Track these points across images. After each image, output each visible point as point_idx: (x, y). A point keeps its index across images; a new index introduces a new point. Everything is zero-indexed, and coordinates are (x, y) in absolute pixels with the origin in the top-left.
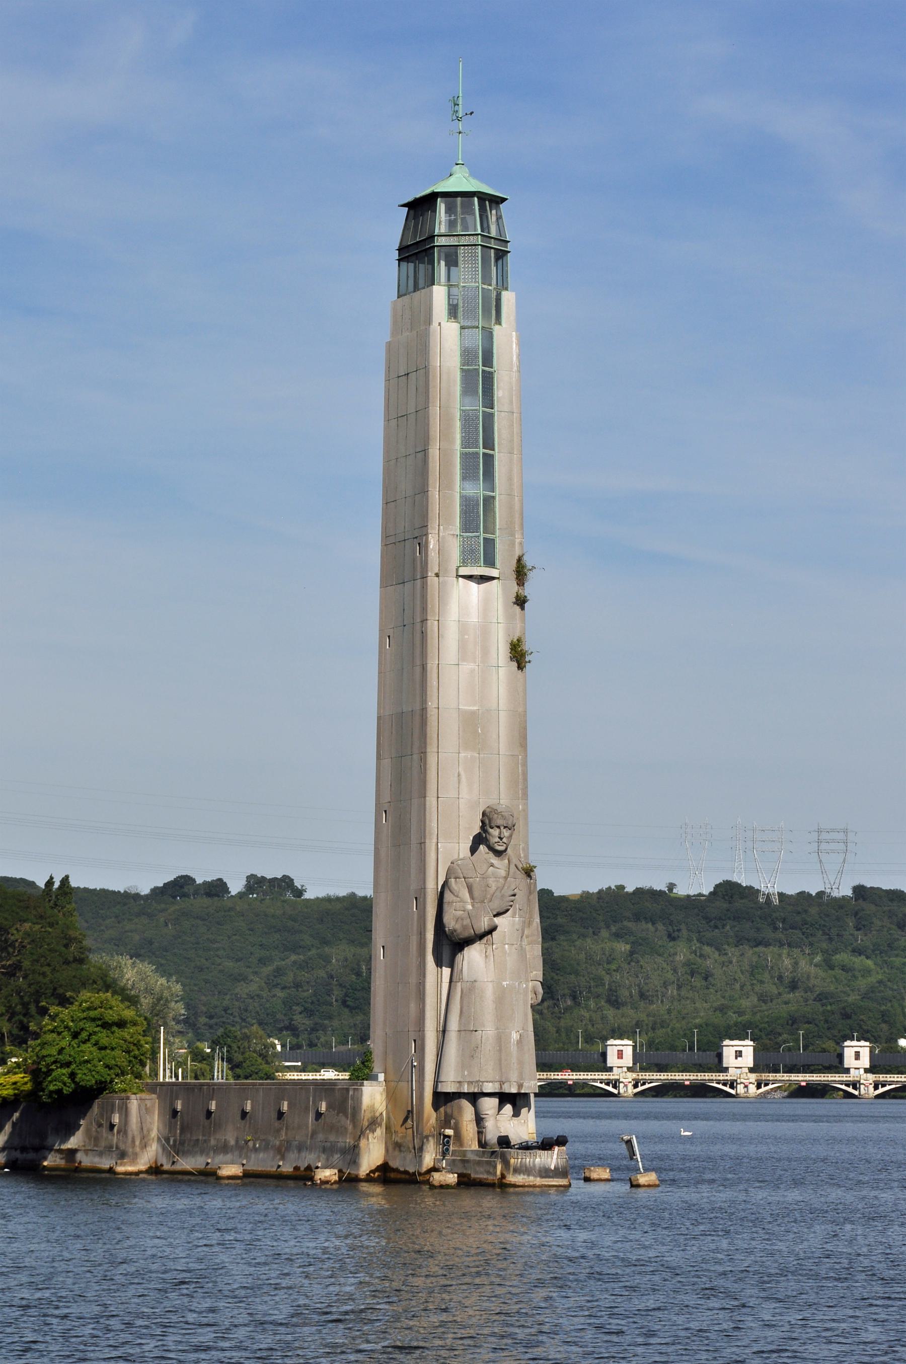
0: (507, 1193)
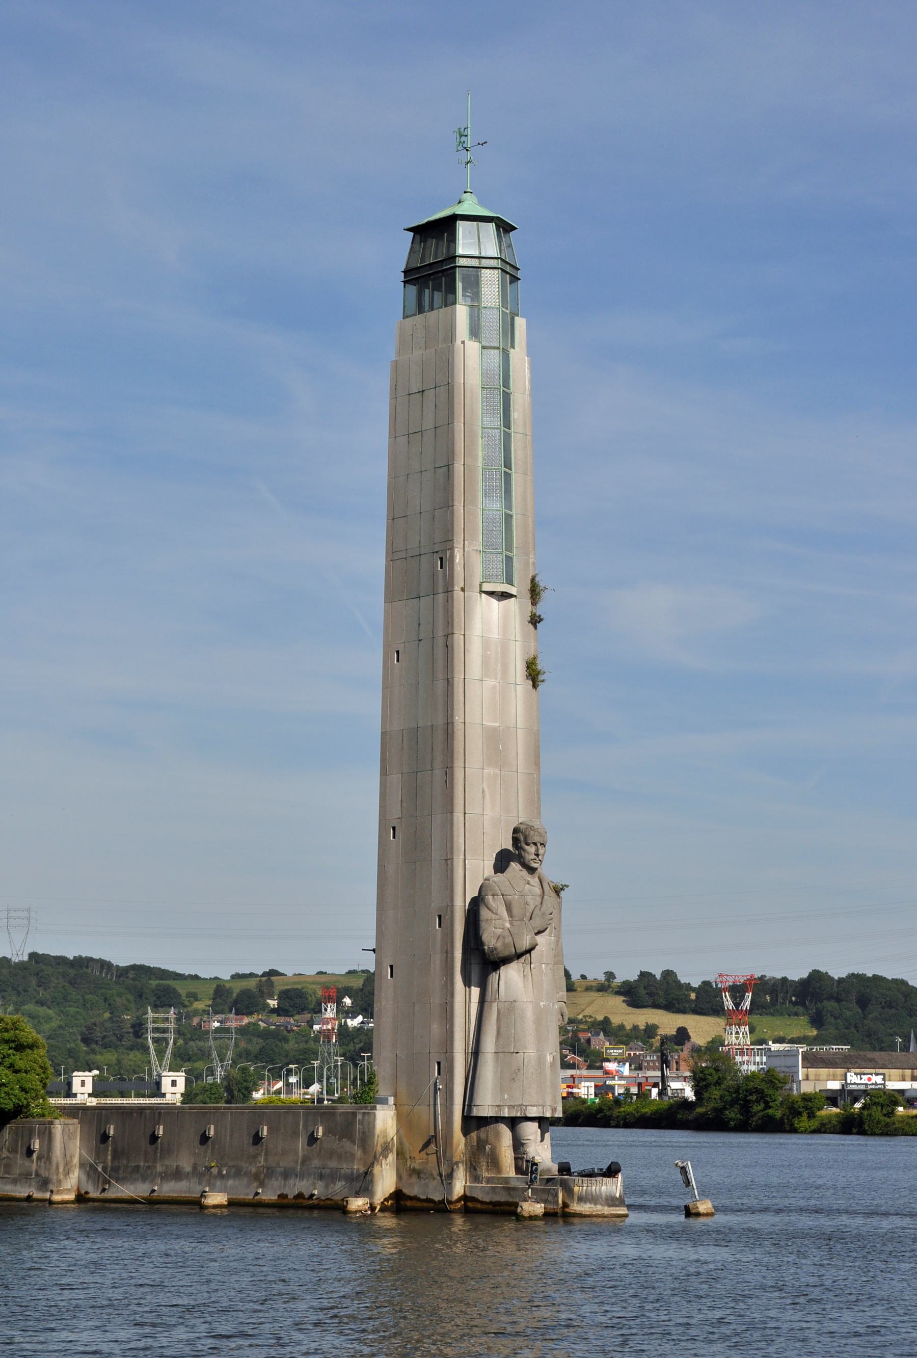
0: (572, 1224)
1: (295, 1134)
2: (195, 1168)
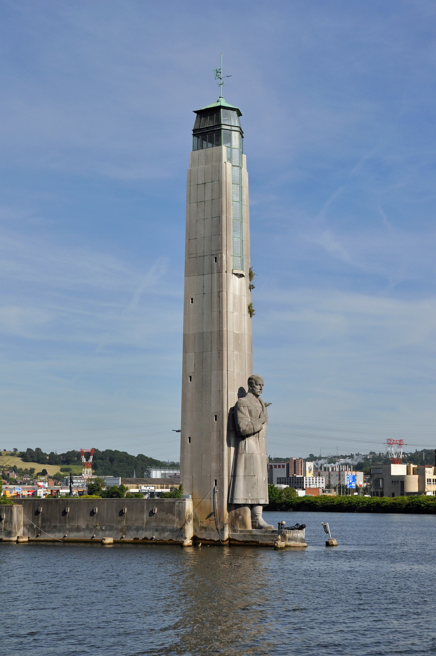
1: (142, 511)
2: (87, 526)
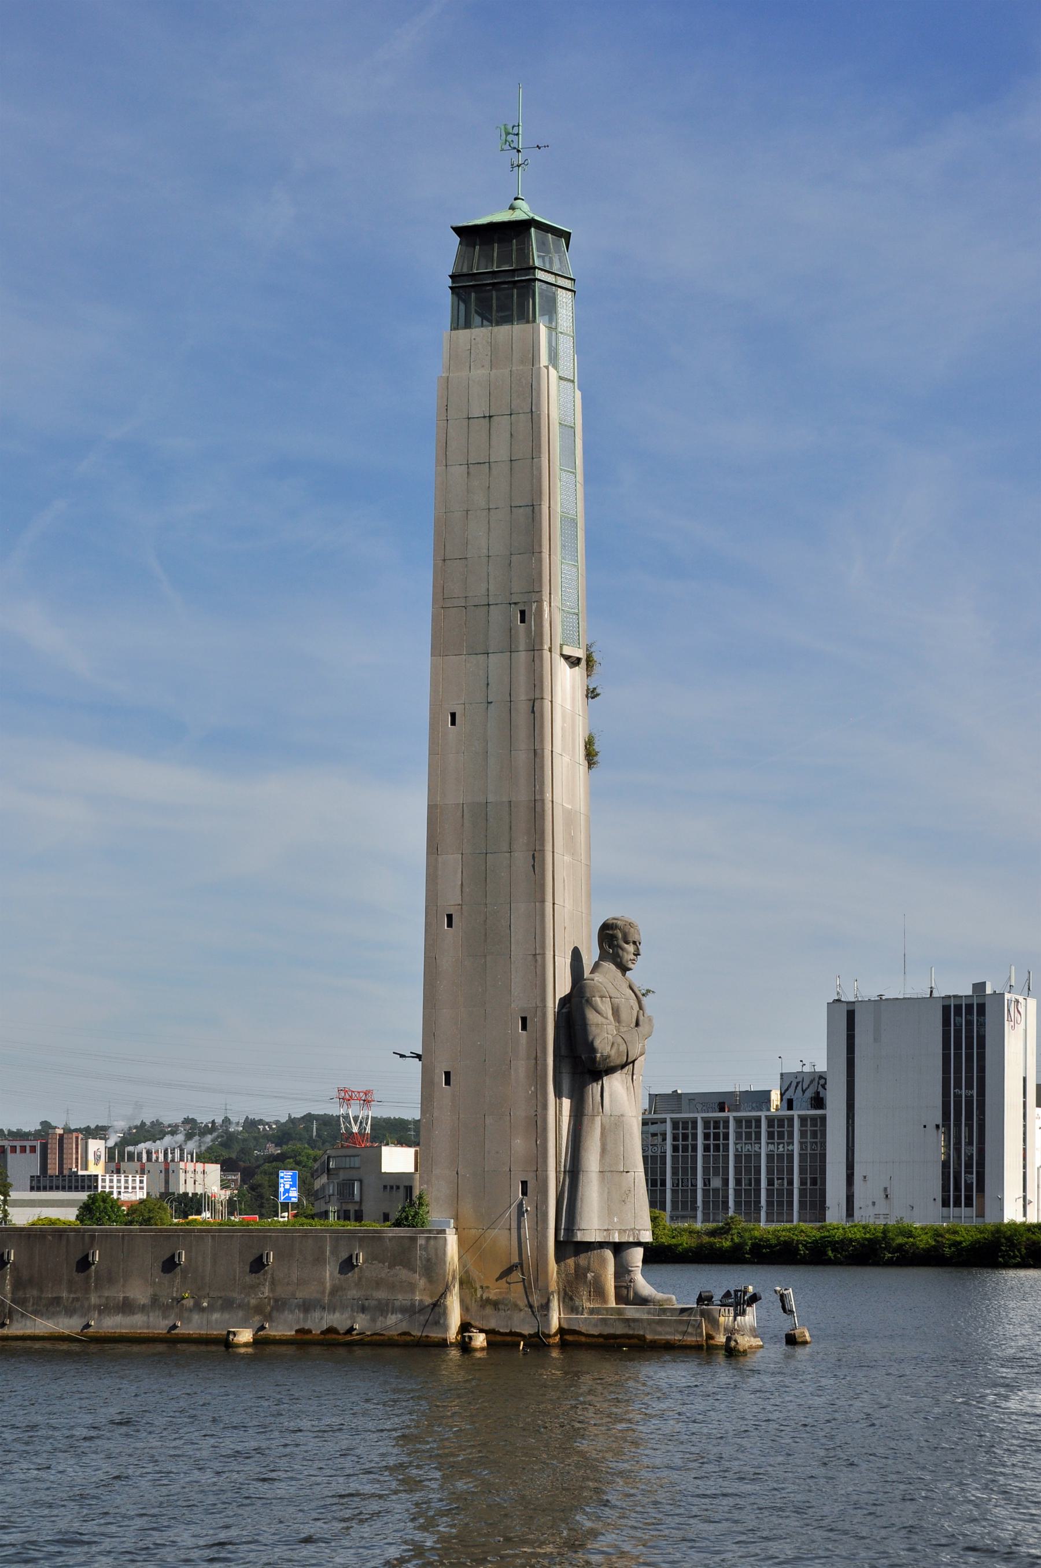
1: (319, 1260)
